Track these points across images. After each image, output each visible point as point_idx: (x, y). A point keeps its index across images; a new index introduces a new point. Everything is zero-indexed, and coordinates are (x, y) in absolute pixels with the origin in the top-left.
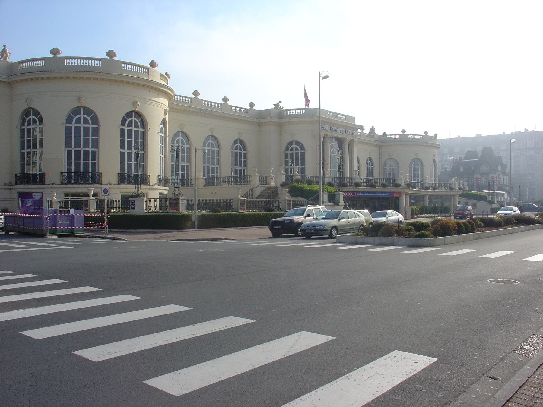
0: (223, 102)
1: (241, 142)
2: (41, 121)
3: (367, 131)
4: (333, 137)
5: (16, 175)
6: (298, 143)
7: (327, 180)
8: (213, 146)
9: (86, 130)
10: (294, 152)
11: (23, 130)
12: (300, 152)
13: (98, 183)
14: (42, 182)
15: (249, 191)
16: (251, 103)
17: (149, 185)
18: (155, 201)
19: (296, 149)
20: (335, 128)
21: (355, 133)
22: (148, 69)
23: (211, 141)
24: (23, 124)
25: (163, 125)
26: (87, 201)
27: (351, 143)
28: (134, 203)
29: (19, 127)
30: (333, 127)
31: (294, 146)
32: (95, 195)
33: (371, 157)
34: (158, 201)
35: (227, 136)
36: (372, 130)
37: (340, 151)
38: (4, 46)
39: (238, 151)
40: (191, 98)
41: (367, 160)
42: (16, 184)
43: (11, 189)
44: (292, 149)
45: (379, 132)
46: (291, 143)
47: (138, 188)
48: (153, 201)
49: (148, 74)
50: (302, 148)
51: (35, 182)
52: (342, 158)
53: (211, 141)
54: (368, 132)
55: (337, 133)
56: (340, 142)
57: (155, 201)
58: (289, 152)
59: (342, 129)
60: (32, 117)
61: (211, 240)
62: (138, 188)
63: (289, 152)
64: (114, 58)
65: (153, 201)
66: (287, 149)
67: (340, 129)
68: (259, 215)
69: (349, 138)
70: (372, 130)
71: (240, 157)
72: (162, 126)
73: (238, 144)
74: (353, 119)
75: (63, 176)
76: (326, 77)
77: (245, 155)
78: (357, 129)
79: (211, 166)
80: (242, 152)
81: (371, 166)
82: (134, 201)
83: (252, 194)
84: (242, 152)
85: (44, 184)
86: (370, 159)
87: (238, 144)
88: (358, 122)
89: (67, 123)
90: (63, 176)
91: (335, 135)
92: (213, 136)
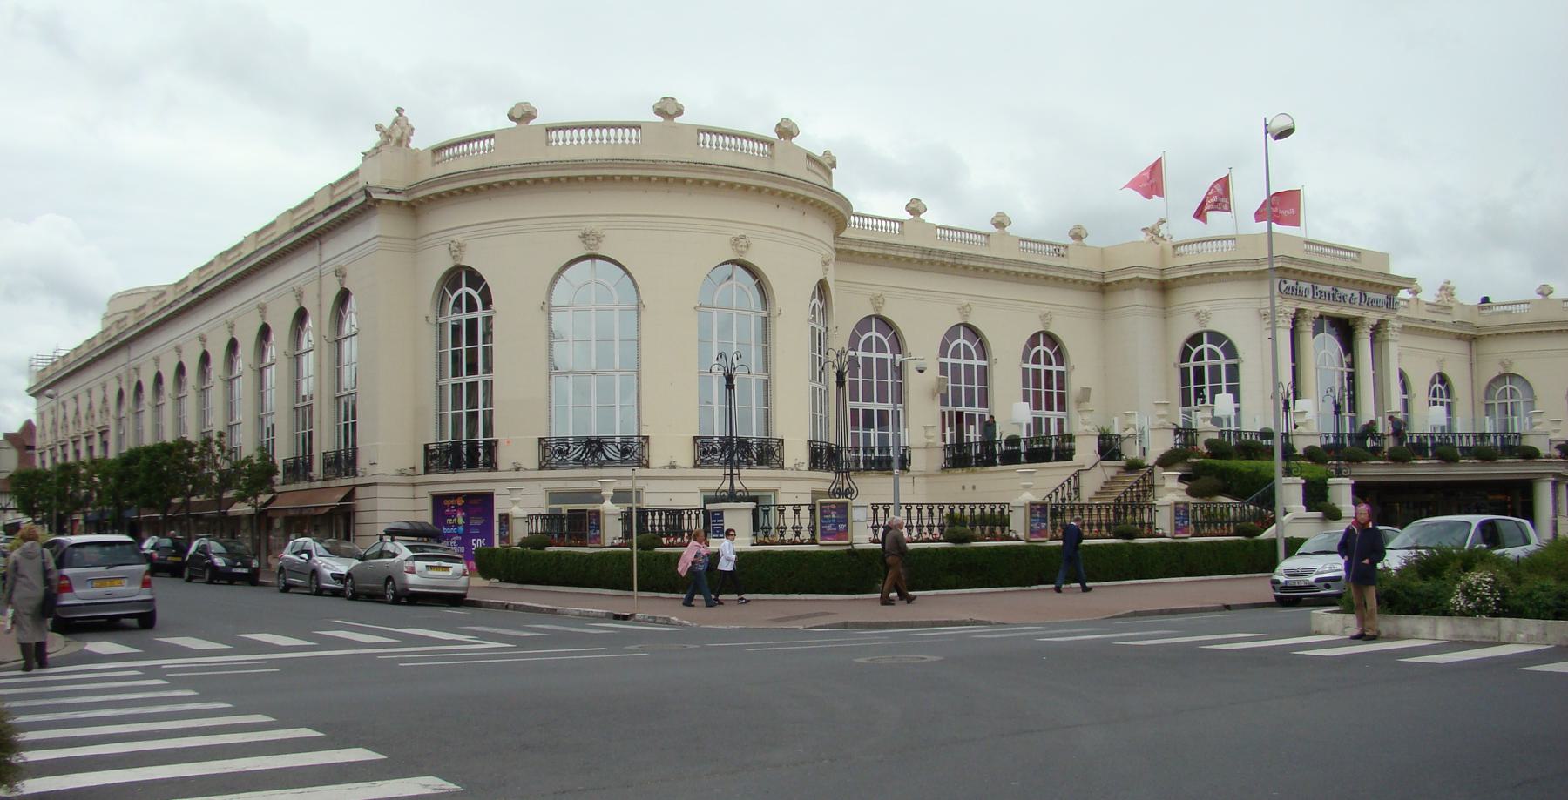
0: (907, 216)
1: (1051, 339)
2: (487, 303)
3: (1428, 295)
4: (1321, 317)
5: (426, 447)
6: (1216, 337)
7: (1300, 446)
8: (968, 355)
9: (1215, 370)
10: (1206, 363)
11: (441, 326)
12: (1223, 361)
13: (640, 465)
14: (491, 465)
15: (1069, 481)
16: (998, 215)
17: (782, 467)
18: (797, 512)
19: (1213, 355)
20: (1327, 289)
21: (1391, 304)
22: (771, 144)
23: (962, 341)
24: (441, 310)
25: (821, 298)
26: (598, 512)
27: (1377, 330)
28: (721, 516)
29: (432, 320)
30: (1322, 288)
31: (1206, 346)
32: (619, 496)
33: (1445, 371)
34: (805, 512)
35: (1008, 324)
36: (1447, 290)
37: (1346, 359)
38: (400, 111)
39: (1043, 367)
40: (902, 223)
41: (1433, 382)
42: (427, 470)
43: (414, 485)
44: (1200, 357)
45: (1468, 297)
46: (1196, 339)
47: (732, 475)
48: (789, 512)
49: (771, 156)
50: (1231, 351)
51: (473, 464)
52: (1352, 378)
53: (962, 341)
54: (1432, 300)
55: (1345, 307)
56: (1345, 330)
57: (797, 512)
58: (1192, 364)
59: (1348, 292)
60: (464, 290)
61: (946, 623)
62: (732, 475)
63: (1192, 364)
64: (677, 120)
65: (789, 512)
66: (1185, 355)
67: (1342, 291)
68: (943, 549)
69: (1372, 317)
70: (1447, 290)
71: (970, 380)
72: (816, 301)
73: (1041, 348)
74: (1384, 258)
75: (545, 447)
76: (1285, 133)
77: (984, 372)
78: (1396, 289)
79: (875, 406)
80: (976, 362)
81: (1054, 368)
82: (721, 512)
83: (1077, 489)
84: (1054, 368)
85: (496, 469)
86: (1443, 379)
87: (1438, 385)
88: (1398, 269)
89: (1236, 366)
90: (545, 447)
91: (1330, 309)
92: (880, 318)
